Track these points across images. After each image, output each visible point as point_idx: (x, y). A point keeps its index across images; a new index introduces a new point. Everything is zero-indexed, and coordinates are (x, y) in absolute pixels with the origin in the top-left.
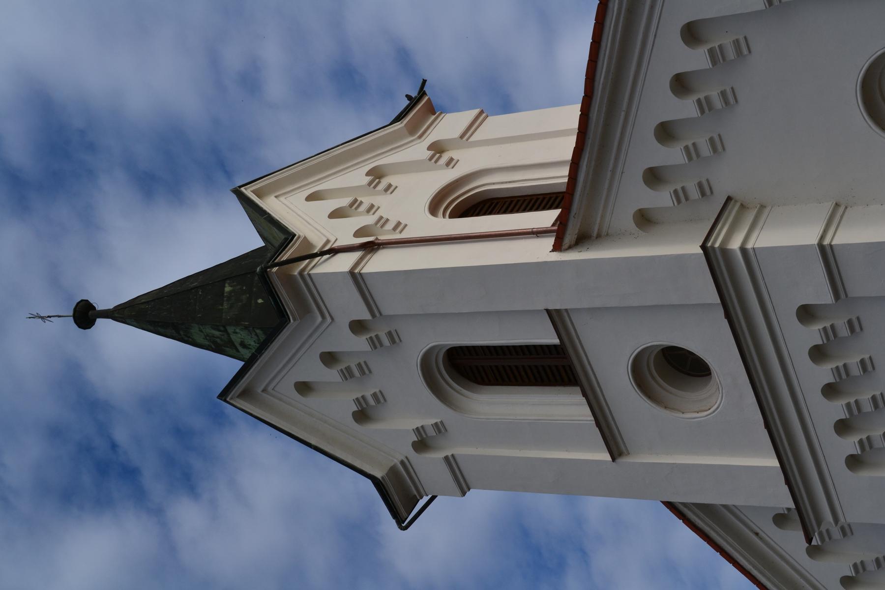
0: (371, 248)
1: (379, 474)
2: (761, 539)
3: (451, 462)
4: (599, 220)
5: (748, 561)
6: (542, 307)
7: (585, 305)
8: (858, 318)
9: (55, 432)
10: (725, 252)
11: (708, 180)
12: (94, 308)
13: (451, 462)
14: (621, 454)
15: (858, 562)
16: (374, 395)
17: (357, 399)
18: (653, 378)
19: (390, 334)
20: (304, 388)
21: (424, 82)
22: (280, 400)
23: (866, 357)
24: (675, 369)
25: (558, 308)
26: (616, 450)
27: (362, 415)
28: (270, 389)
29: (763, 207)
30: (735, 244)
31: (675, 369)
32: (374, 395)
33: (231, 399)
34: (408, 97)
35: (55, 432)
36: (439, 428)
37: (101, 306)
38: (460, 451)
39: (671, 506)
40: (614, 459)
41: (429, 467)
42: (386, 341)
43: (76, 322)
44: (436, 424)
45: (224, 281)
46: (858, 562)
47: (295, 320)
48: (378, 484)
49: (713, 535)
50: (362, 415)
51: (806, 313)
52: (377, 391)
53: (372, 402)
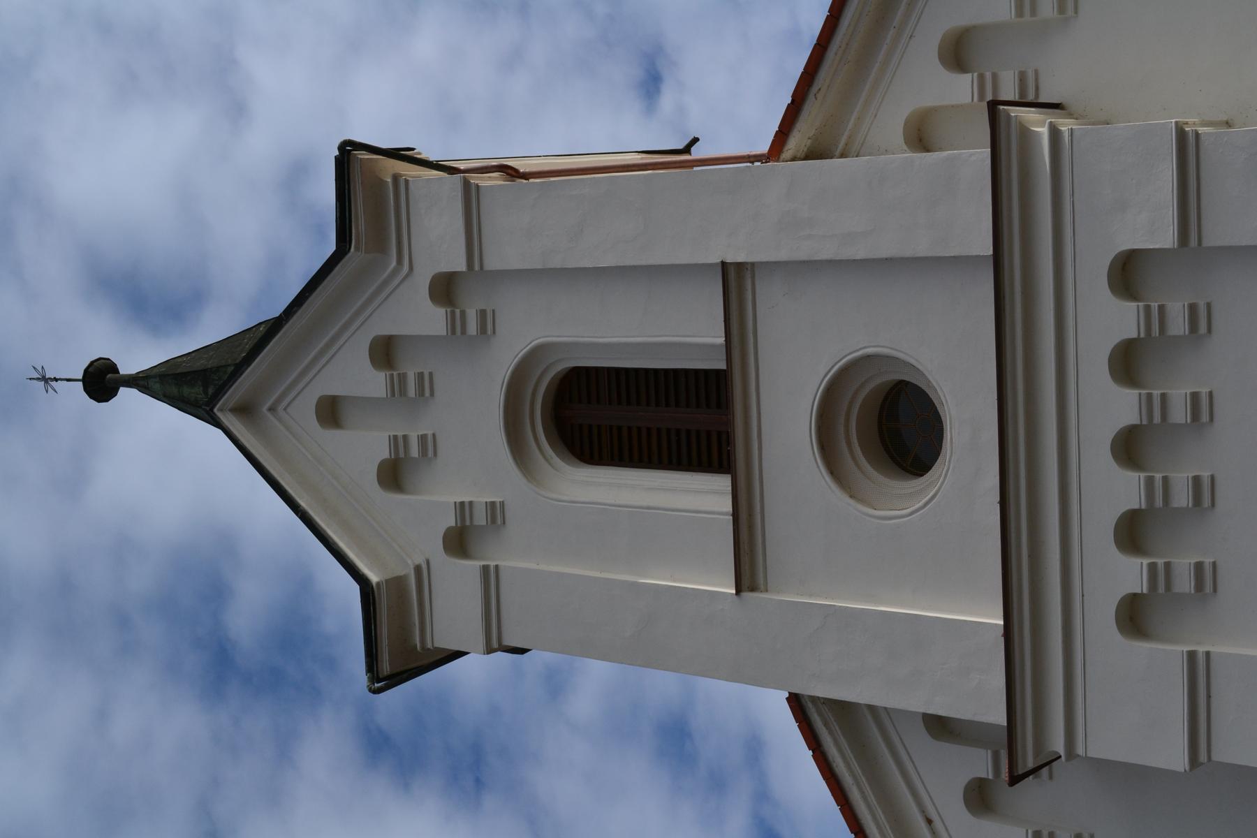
1: (374, 578)
4: (850, 125)
6: (715, 259)
7: (783, 255)
8: (1209, 306)
11: (1036, 72)
12: (117, 371)
14: (753, 589)
16: (423, 439)
17: (395, 437)
18: (849, 443)
19: (482, 314)
21: (695, 140)
22: (288, 428)
23: (1208, 561)
24: (892, 427)
25: (741, 258)
28: (280, 408)
31: (892, 427)
32: (423, 439)
33: (221, 410)
36: (496, 512)
37: (129, 366)
41: (453, 609)
43: (86, 390)
44: (493, 503)
47: (357, 249)
49: (855, 796)
52: (430, 433)
53: (414, 451)
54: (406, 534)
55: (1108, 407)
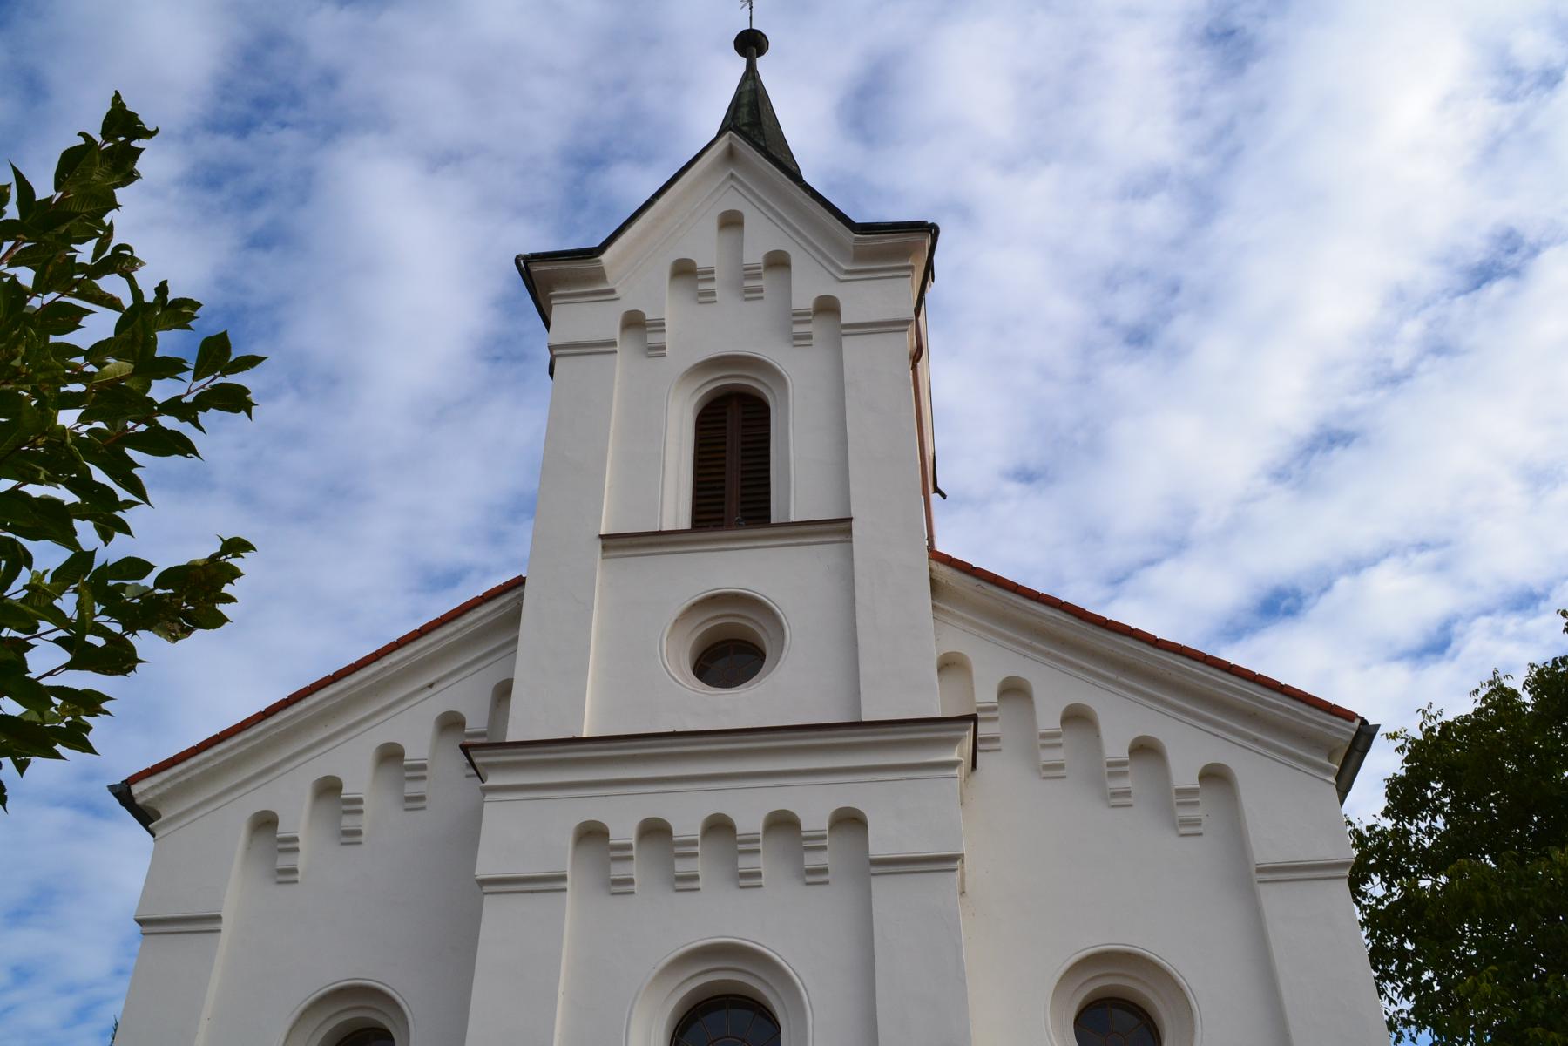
1: (605, 258)
2: (422, 689)
5: (397, 663)
9: (330, 79)
14: (604, 548)
15: (362, 807)
16: (712, 293)
20: (731, 221)
25: (854, 531)
26: (612, 542)
35: (330, 79)
37: (762, 63)
40: (602, 537)
46: (362, 807)
55: (749, 810)
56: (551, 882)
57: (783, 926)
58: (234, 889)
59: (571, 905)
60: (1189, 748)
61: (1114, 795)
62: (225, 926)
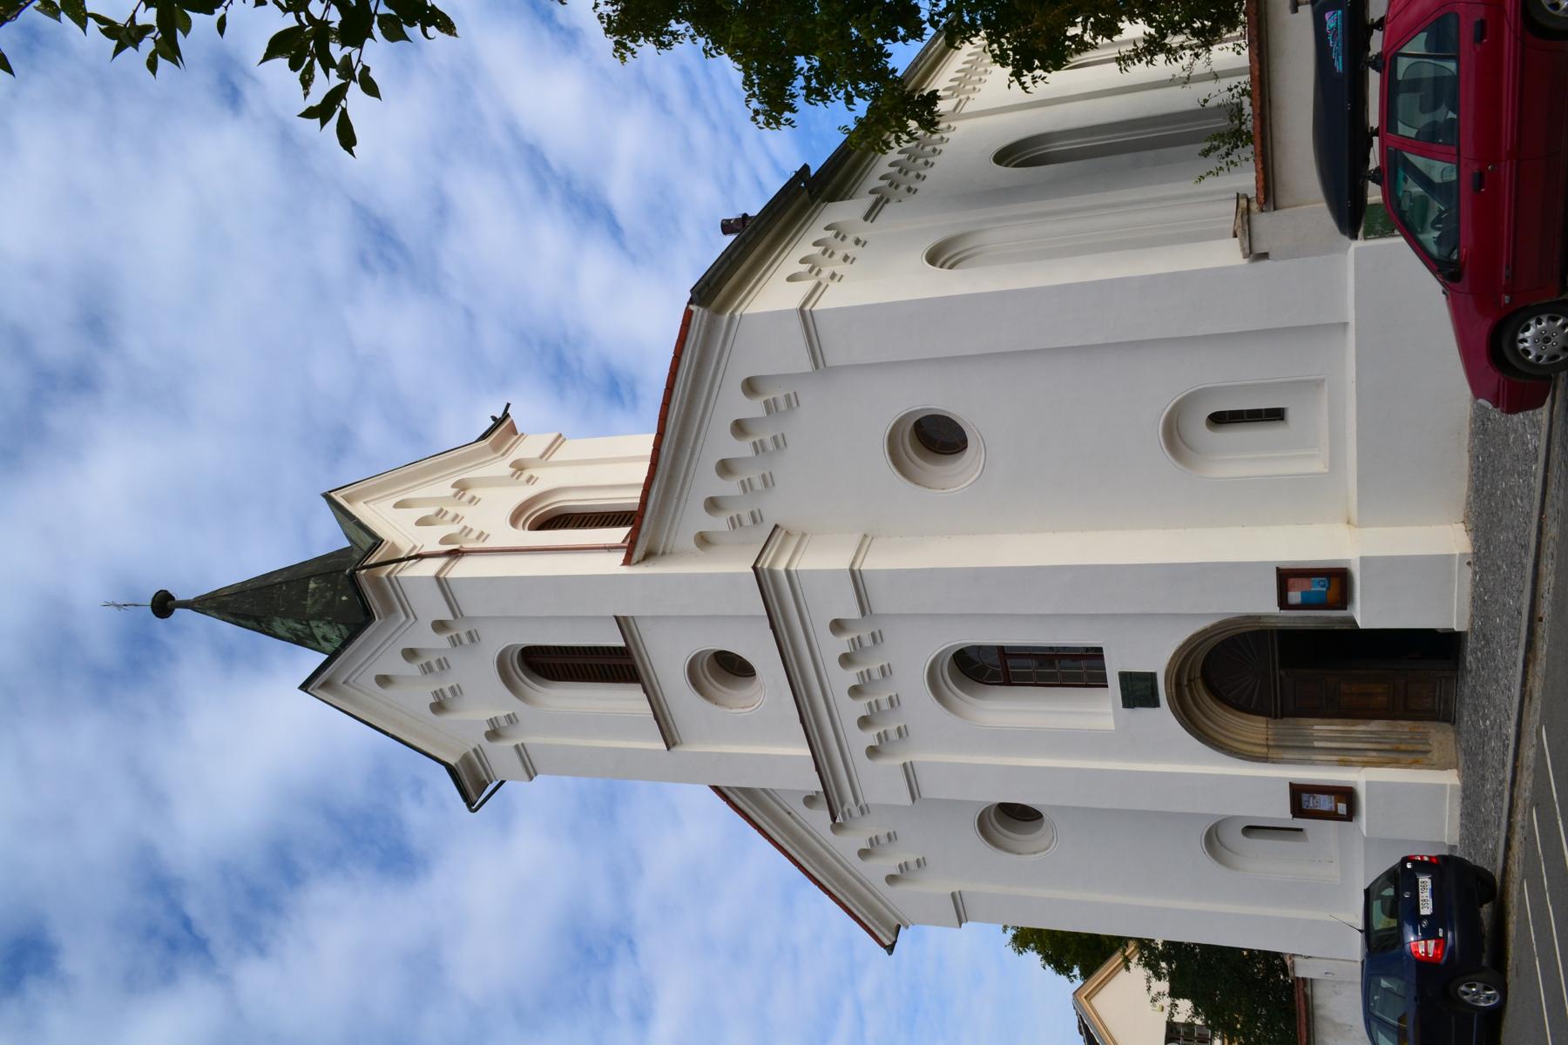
0: (455, 554)
1: (452, 761)
3: (520, 750)
7: (649, 613)
10: (772, 572)
13: (520, 750)
14: (675, 744)
16: (452, 689)
20: (384, 680)
24: (730, 668)
26: (670, 741)
27: (439, 707)
29: (804, 535)
30: (780, 567)
31: (730, 668)
32: (452, 689)
34: (494, 418)
36: (511, 719)
37: (180, 596)
38: (530, 740)
39: (716, 789)
41: (500, 757)
42: (465, 640)
45: (308, 578)
48: (452, 771)
49: (752, 815)
50: (439, 707)
51: (838, 626)
53: (449, 695)
54: (462, 731)
55: (841, 680)
56: (908, 770)
57: (912, 656)
58: (937, 886)
59: (920, 757)
60: (730, 403)
61: (777, 446)
62: (956, 887)
